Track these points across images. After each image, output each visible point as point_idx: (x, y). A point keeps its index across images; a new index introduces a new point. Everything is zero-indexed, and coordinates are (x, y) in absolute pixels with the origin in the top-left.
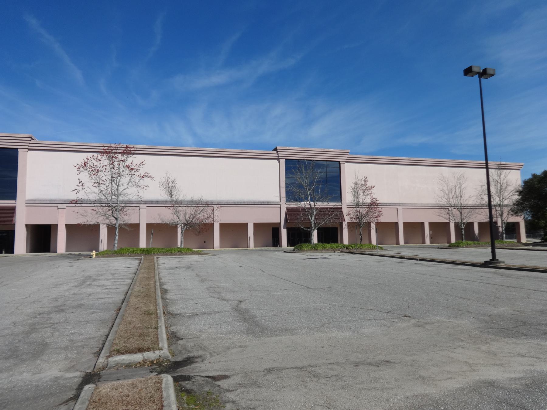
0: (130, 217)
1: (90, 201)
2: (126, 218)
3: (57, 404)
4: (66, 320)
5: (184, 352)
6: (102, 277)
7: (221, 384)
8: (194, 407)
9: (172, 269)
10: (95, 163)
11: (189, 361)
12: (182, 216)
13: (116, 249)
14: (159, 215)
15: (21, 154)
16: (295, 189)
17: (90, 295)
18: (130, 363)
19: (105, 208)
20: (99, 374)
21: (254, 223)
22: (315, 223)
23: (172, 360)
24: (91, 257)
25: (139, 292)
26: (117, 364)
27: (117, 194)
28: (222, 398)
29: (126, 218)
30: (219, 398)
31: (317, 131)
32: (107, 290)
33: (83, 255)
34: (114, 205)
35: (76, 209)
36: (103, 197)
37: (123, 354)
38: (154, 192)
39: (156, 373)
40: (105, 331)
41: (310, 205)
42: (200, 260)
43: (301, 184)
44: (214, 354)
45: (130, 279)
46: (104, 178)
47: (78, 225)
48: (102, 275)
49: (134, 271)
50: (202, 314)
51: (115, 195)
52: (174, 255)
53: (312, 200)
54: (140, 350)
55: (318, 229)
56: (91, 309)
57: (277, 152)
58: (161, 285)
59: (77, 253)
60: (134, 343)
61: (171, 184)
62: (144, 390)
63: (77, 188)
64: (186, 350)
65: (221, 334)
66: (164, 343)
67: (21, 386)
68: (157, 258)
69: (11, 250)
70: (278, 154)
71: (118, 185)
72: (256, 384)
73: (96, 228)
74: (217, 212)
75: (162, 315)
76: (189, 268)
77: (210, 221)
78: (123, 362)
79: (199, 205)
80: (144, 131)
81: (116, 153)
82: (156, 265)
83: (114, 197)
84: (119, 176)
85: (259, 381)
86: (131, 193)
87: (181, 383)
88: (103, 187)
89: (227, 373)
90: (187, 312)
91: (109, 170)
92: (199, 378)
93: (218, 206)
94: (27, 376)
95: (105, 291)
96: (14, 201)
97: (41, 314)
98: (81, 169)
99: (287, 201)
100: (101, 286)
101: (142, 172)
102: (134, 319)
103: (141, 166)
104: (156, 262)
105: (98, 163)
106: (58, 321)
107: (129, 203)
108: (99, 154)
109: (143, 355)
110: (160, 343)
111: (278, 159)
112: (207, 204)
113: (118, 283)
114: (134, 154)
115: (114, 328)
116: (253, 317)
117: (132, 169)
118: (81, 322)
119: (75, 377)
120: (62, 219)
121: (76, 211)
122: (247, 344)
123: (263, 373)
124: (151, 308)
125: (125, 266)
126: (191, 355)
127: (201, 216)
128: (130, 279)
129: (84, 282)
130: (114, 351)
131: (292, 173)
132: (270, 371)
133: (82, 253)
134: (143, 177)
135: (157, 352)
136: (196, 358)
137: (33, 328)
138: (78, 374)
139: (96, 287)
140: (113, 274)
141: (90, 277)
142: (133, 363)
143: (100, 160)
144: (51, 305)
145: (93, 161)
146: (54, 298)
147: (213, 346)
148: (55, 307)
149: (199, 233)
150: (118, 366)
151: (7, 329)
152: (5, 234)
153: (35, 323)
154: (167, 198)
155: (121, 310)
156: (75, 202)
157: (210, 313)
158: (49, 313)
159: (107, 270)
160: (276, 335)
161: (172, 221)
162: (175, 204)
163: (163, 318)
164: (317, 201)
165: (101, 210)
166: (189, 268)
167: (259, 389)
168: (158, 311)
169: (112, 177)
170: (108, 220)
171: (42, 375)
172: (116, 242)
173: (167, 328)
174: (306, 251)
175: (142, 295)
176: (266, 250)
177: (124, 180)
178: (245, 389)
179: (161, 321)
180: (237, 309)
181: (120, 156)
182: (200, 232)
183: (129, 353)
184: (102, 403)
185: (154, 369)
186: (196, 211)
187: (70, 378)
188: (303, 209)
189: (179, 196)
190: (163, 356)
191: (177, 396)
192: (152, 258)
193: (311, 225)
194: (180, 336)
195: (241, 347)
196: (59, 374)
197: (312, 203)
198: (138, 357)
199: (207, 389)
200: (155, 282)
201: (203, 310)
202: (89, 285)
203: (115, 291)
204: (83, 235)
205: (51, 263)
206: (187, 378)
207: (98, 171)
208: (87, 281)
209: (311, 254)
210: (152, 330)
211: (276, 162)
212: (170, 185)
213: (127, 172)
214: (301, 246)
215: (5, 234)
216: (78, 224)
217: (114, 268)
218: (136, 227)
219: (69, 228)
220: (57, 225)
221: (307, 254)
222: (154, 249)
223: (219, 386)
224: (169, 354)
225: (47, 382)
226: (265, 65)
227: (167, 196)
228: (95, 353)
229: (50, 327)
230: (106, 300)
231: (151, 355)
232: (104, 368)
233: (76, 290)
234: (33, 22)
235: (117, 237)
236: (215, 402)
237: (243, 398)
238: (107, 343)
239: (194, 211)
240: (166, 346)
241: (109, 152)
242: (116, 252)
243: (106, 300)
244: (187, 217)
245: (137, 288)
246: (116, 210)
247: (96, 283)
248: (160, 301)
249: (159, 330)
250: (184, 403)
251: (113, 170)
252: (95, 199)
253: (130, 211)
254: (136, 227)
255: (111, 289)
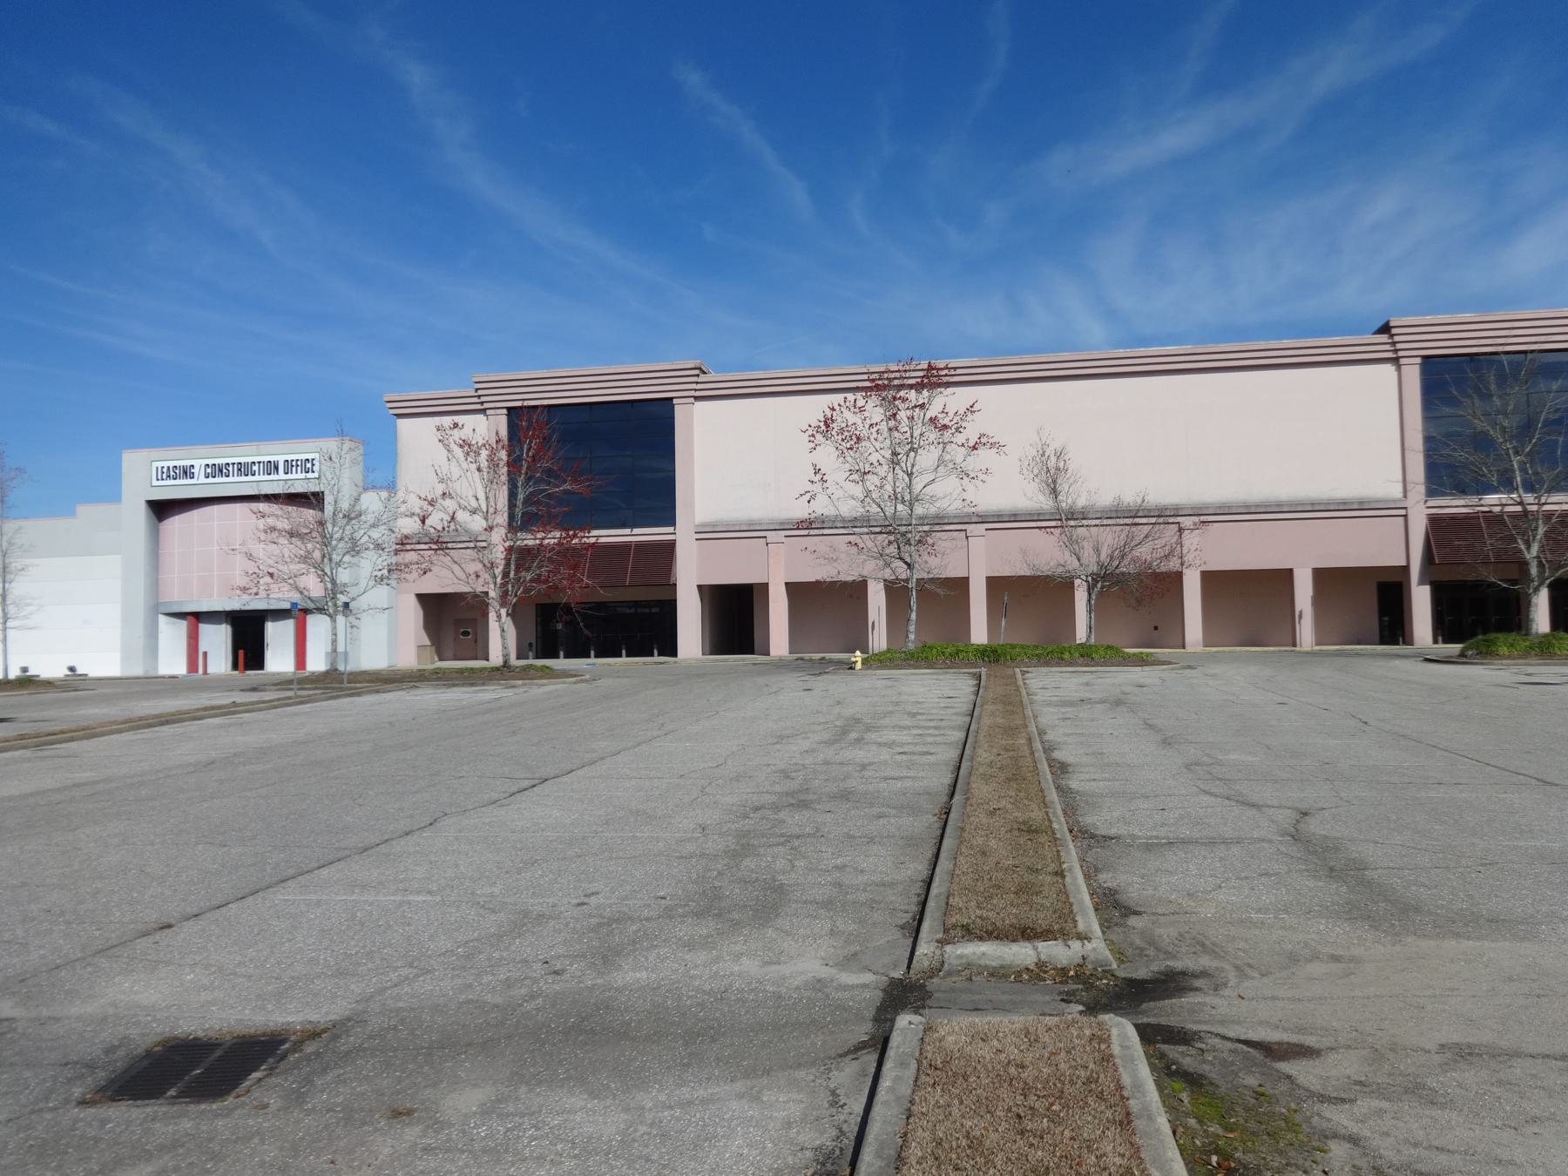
0: (944, 559)
1: (843, 520)
2: (933, 562)
3: (833, 1053)
4: (818, 830)
5: (1151, 952)
6: (887, 721)
7: (1293, 1073)
8: (1220, 1132)
9: (1071, 704)
10: (851, 418)
11: (1171, 984)
12: (1088, 555)
13: (911, 646)
14: (1024, 552)
15: (680, 412)
16: (1461, 455)
17: (864, 767)
18: (1002, 967)
19: (880, 537)
20: (923, 986)
21: (1203, 573)
22: (1541, 565)
23: (1122, 974)
24: (851, 667)
25: (991, 765)
26: (968, 966)
27: (907, 498)
28: (1308, 1120)
29: (933, 562)
30: (1298, 1118)
31: (1528, 256)
32: (904, 757)
33: (831, 661)
34: (903, 529)
35: (811, 542)
36: (874, 509)
37: (981, 939)
38: (1007, 486)
39: (1081, 1008)
40: (920, 868)
41: (1521, 503)
42: (1148, 681)
43: (1486, 434)
44: (1248, 971)
45: (959, 728)
46: (874, 458)
47: (817, 584)
48: (886, 715)
49: (967, 707)
50: (1183, 842)
51: (903, 502)
52: (1070, 664)
53: (1529, 487)
54: (1027, 933)
55: (1550, 587)
56: (872, 805)
57: (1392, 336)
58: (1048, 750)
59: (817, 656)
60: (1007, 911)
61: (1052, 463)
62: (1063, 1054)
63: (809, 487)
64: (1158, 949)
65: (1259, 911)
66: (1088, 920)
67: (740, 991)
68: (1024, 673)
69: (670, 648)
70: (1394, 343)
71: (910, 475)
72: (1415, 1090)
73: (857, 590)
74: (1191, 540)
75: (1068, 836)
76: (1118, 703)
77: (1174, 564)
78: (982, 962)
79: (1137, 520)
80: (962, 321)
81: (901, 387)
82: (1024, 692)
83: (900, 507)
84: (912, 449)
85: (1431, 1082)
86: (945, 494)
87: (1165, 1047)
88: (872, 481)
89: (1310, 1041)
90: (1136, 832)
91: (886, 434)
92: (1217, 1040)
93: (1196, 519)
94: (750, 966)
95: (899, 758)
96: (671, 529)
97: (757, 809)
98: (819, 436)
99: (1431, 493)
100: (890, 745)
101: (971, 433)
102: (993, 843)
103: (970, 417)
104: (1020, 683)
105: (857, 419)
106: (796, 830)
107: (940, 521)
108: (859, 395)
109: (1036, 949)
110: (1078, 918)
111: (1395, 361)
112: (1165, 515)
113: (930, 739)
114: (949, 385)
115: (944, 864)
116: (1360, 866)
117: (945, 427)
118: (853, 837)
119: (865, 986)
120: (776, 570)
121: (811, 549)
122: (1356, 951)
123: (1437, 1059)
124: (1033, 815)
125: (941, 693)
126: (1178, 965)
127: (1144, 552)
128: (959, 728)
129: (845, 731)
130: (954, 926)
131: (1453, 402)
132: (1464, 1054)
133: (828, 656)
134: (974, 448)
135: (1076, 945)
136: (1195, 976)
137: (744, 847)
138: (868, 978)
139: (874, 747)
140: (914, 715)
141: (858, 721)
142: (1010, 966)
143: (862, 409)
144: (778, 788)
145: (847, 414)
146: (782, 771)
147: (1242, 945)
148: (787, 794)
149: (1139, 602)
150: (970, 970)
151: (689, 840)
152: (655, 610)
153: (749, 832)
154: (1043, 502)
155: (952, 815)
156: (807, 525)
157: (1211, 843)
158: (776, 808)
159: (897, 704)
160: (1457, 935)
161: (1061, 569)
162: (1066, 519)
163: (1071, 846)
164: (1549, 491)
165: (870, 544)
166: (1118, 703)
167: (1436, 1113)
168: (1055, 826)
169: (895, 454)
170: (888, 571)
171: (785, 970)
172: (912, 628)
173: (1087, 876)
174: (1509, 657)
175: (1002, 776)
176: (1358, 655)
177: (927, 458)
178: (1385, 1105)
179: (1068, 852)
180: (1296, 836)
181: (912, 394)
182: (1141, 598)
183: (997, 938)
184: (955, 1075)
185: (1072, 993)
186: (1130, 537)
187: (853, 987)
188: (1494, 520)
189: (1079, 495)
190: (1092, 957)
191: (1160, 1088)
192: (1010, 671)
193: (1527, 572)
194: (1132, 904)
195: (1336, 959)
196: (825, 972)
197: (1529, 498)
198: (1021, 953)
199: (1252, 1081)
200: (1030, 740)
201: (1185, 832)
202: (858, 740)
203: (925, 759)
204: (828, 607)
205: (761, 680)
206: (1182, 1037)
207: (858, 439)
208: (849, 730)
209: (1530, 670)
210: (1048, 879)
211: (1389, 369)
212: (1052, 463)
213: (933, 435)
214: (1490, 643)
215: (655, 610)
216: (818, 582)
217: (912, 699)
218: (961, 585)
219: (795, 590)
220: (766, 585)
221: (1514, 669)
222: (1013, 647)
223: (1289, 1077)
224: (1108, 953)
225: (798, 988)
226: (1336, 65)
227: (1042, 498)
228: (902, 927)
229: (782, 844)
230: (908, 783)
231: (1058, 952)
232: (934, 972)
233: (829, 753)
234: (693, 79)
235: (914, 616)
236: (1289, 1130)
237: (1387, 1134)
238: (931, 904)
239: (1123, 536)
240: (1096, 929)
241: (885, 387)
242: (912, 655)
243: (908, 783)
244: (1103, 556)
245: (984, 755)
246: (908, 543)
247: (873, 736)
248: (1053, 796)
249: (1068, 880)
250: (1187, 1115)
251: (896, 434)
252: (854, 514)
253: (944, 544)
254: (961, 585)
255: (913, 753)
